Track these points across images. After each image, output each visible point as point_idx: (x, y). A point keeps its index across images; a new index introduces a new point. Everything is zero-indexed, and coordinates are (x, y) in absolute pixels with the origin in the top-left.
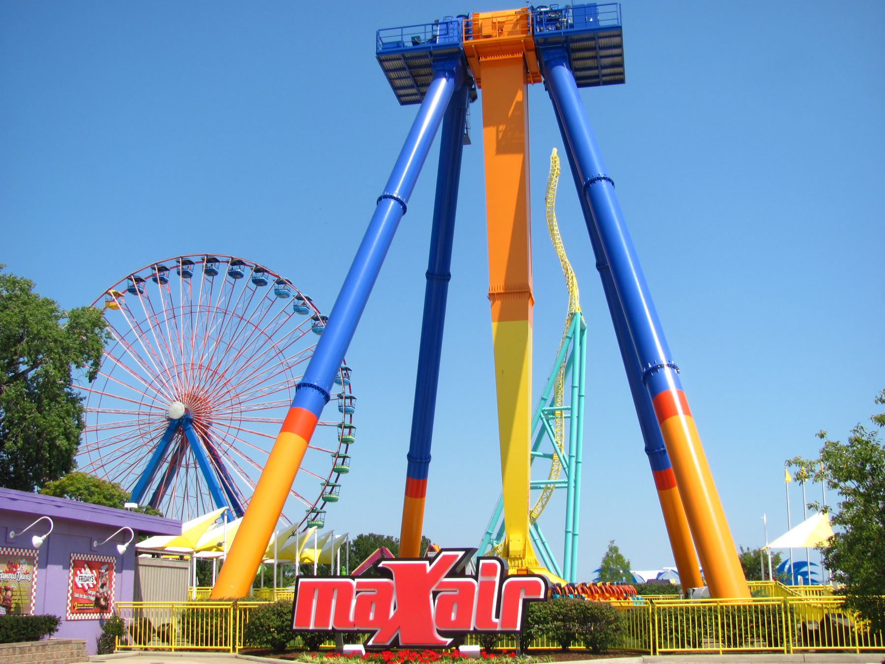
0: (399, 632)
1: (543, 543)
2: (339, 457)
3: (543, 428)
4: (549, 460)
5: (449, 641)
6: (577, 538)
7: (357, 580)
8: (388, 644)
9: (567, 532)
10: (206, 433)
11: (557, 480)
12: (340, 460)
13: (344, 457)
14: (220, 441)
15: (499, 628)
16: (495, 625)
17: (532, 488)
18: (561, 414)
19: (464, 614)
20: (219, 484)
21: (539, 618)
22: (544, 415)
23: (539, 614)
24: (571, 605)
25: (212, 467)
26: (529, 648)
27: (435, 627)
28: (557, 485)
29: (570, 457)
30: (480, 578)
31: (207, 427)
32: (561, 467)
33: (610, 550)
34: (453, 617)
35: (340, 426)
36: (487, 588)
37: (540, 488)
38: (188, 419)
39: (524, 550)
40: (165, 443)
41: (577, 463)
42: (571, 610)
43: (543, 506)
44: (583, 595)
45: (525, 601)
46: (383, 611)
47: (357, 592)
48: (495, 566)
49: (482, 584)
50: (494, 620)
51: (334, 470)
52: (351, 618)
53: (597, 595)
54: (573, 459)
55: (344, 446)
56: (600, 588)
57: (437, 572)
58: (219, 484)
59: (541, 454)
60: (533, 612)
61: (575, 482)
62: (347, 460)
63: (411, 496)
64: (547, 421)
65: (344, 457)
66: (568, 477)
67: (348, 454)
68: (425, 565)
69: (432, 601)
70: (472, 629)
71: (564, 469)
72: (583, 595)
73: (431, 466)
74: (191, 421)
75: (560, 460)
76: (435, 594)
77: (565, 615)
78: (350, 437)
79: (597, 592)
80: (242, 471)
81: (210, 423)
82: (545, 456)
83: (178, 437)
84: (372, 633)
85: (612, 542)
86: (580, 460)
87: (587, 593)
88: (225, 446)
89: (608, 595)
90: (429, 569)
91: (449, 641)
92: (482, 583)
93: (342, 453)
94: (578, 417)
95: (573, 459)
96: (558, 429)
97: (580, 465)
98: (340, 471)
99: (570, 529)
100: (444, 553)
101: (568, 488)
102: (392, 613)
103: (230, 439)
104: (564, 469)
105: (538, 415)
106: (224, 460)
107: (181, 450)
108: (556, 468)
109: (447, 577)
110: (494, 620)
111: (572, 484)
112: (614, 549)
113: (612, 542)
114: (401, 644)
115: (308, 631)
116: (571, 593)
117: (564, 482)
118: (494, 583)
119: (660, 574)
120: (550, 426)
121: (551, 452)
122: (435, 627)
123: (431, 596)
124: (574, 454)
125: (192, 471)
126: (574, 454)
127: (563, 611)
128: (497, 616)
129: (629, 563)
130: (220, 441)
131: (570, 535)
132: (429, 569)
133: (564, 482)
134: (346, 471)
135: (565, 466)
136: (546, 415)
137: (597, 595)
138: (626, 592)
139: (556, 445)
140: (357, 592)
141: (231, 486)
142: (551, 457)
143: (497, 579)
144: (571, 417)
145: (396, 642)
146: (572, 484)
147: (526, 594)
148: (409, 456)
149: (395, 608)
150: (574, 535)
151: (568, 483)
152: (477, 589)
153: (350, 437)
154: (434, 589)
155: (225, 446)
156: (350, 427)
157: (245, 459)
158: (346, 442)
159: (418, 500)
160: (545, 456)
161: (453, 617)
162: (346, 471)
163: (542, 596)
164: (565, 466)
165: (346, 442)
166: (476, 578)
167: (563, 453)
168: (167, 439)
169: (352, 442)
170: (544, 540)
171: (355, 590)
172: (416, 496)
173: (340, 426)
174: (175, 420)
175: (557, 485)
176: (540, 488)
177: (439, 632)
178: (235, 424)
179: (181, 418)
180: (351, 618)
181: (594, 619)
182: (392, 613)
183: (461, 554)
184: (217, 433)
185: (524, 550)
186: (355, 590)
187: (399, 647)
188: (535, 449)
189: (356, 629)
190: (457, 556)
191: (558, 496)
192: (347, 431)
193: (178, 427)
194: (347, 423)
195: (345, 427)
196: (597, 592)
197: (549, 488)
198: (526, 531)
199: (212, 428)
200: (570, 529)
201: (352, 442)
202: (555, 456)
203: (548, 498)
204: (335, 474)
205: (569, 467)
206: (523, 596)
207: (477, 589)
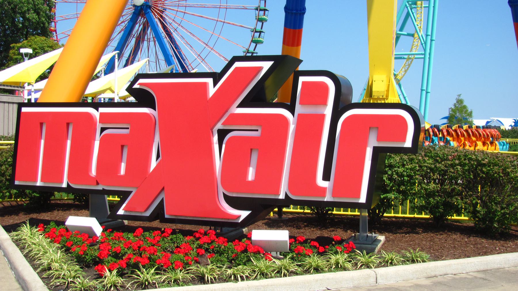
0: (162, 196)
1: (404, 98)
2: (256, 32)
3: (408, 15)
4: (412, 38)
5: (244, 214)
6: (429, 94)
7: (102, 110)
8: (148, 214)
9: (422, 90)
10: (162, 17)
11: (417, 53)
12: (257, 34)
13: (260, 32)
14: (171, 21)
15: (328, 198)
16: (323, 190)
17: (396, 58)
18: (422, 5)
19: (270, 171)
20: (171, 52)
21: (402, 176)
22: (409, 4)
23: (401, 170)
24: (454, 158)
25: (166, 41)
26: (385, 215)
27: (221, 190)
28: (416, 56)
29: (427, 35)
30: (299, 109)
31: (162, 12)
32: (419, 44)
33: (457, 102)
34: (251, 175)
35: (257, 9)
36: (309, 127)
37: (404, 58)
38: (147, 5)
39: (388, 91)
40: (132, 24)
41: (431, 40)
42: (453, 166)
43: (406, 71)
44: (449, 138)
45: (376, 150)
46: (139, 162)
47: (103, 130)
48: (325, 87)
49: (302, 119)
50: (321, 182)
51: (252, 41)
52: (93, 172)
53: (462, 139)
54: (429, 38)
55: (260, 24)
56: (466, 131)
57: (224, 98)
58: (171, 52)
59: (406, 33)
60: (391, 166)
61: (430, 54)
62: (262, 34)
63: (288, 45)
64: (411, 9)
65: (260, 32)
66: (425, 50)
67: (263, 30)
68: (205, 84)
69: (216, 147)
70: (282, 196)
71: (422, 44)
72: (449, 138)
73: (307, 18)
74: (150, 7)
75: (419, 38)
76: (222, 134)
77: (444, 173)
78: (264, 17)
79: (463, 135)
80: (187, 43)
81: (165, 9)
82: (408, 35)
83: (141, 20)
84: (124, 195)
85: (459, 95)
86: (434, 38)
87: (452, 136)
88: (175, 25)
89: (474, 139)
90: (212, 91)
91: (244, 214)
92: (301, 117)
93: (259, 28)
94: (434, 7)
95: (429, 38)
96: (418, 16)
97: (434, 42)
98: (257, 42)
99: (424, 88)
100: (238, 64)
101: (424, 58)
102: (154, 164)
103: (178, 20)
104: (422, 44)
105: (404, 5)
106: (175, 35)
107: (144, 30)
108: (416, 44)
109: (241, 106)
110: (321, 182)
111: (427, 56)
112: (460, 101)
113: (459, 95)
114: (167, 216)
115: (35, 188)
116: (435, 135)
117: (422, 54)
118: (322, 117)
119: (488, 122)
120: (413, 13)
121: (412, 32)
122: (221, 190)
123: (215, 138)
124: (429, 33)
125: (152, 43)
126: (429, 33)
127: (441, 166)
128: (326, 177)
129: (471, 112)
130: (171, 21)
131: (424, 92)
132: (212, 91)
133: (422, 54)
134: (261, 42)
135: (423, 42)
136: (410, 5)
137: (462, 139)
138: (492, 137)
139: (417, 27)
140: (103, 130)
141: (180, 54)
142: (413, 35)
143: (328, 111)
144: (429, 7)
145: (158, 214)
146: (427, 56)
147: (379, 139)
148: (286, 9)
149: (158, 157)
150: (427, 93)
151: (424, 54)
152: (292, 127)
153: (264, 17)
154: (219, 126)
155: (175, 25)
156: (265, 10)
157: (189, 34)
158: (262, 21)
159: (295, 48)
160: (408, 35)
161: (251, 175)
162: (261, 42)
163: (408, 144)
164: (423, 42)
165: (262, 21)
166: (291, 109)
167: (422, 33)
168: (133, 21)
169: (266, 21)
170: (405, 95)
171: (99, 126)
172: (293, 45)
173: (257, 9)
174: (138, 7)
175: (416, 56)
176: (404, 58)
177: (230, 201)
178: (182, 9)
179: (142, 5)
180: (93, 172)
181: (493, 182)
182: (154, 164)
183: (266, 65)
184: (169, 15)
185: (388, 91)
186: (99, 126)
187: (164, 220)
188: (401, 30)
189: (100, 187)
190: (260, 69)
191: (417, 64)
192: (262, 13)
193: (140, 11)
194: (262, 7)
195: (261, 10)
196: (463, 135)
197: (410, 58)
198: (390, 72)
199: (166, 13)
200: (424, 88)
201: (266, 21)
202: (416, 35)
203: (409, 65)
204: (253, 45)
205: (425, 43)
206: (373, 142)
207: (292, 127)
